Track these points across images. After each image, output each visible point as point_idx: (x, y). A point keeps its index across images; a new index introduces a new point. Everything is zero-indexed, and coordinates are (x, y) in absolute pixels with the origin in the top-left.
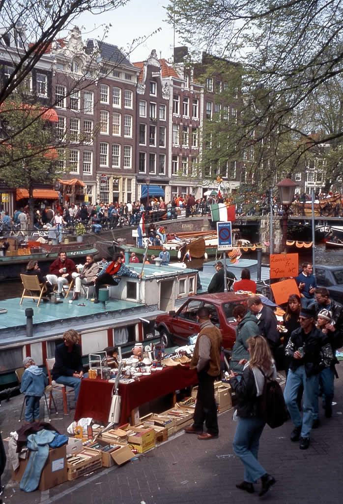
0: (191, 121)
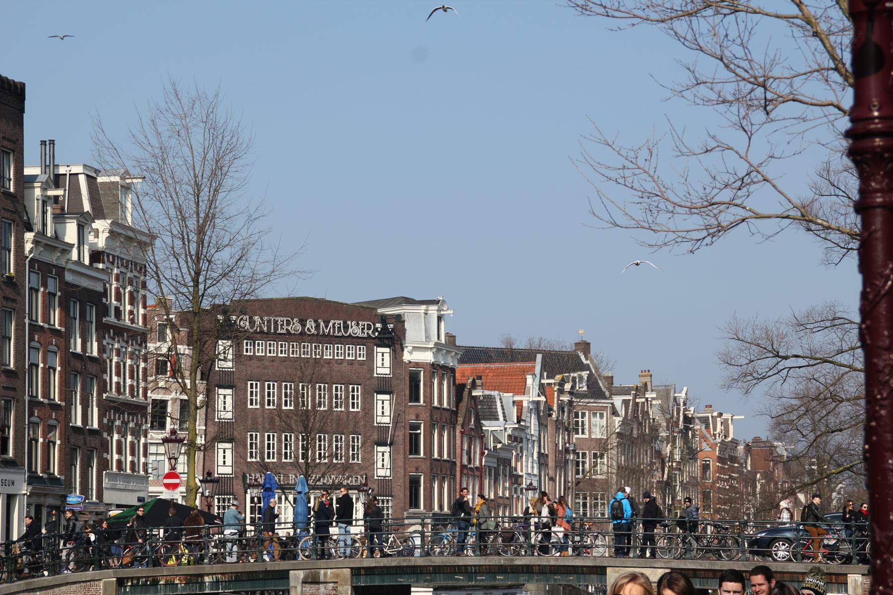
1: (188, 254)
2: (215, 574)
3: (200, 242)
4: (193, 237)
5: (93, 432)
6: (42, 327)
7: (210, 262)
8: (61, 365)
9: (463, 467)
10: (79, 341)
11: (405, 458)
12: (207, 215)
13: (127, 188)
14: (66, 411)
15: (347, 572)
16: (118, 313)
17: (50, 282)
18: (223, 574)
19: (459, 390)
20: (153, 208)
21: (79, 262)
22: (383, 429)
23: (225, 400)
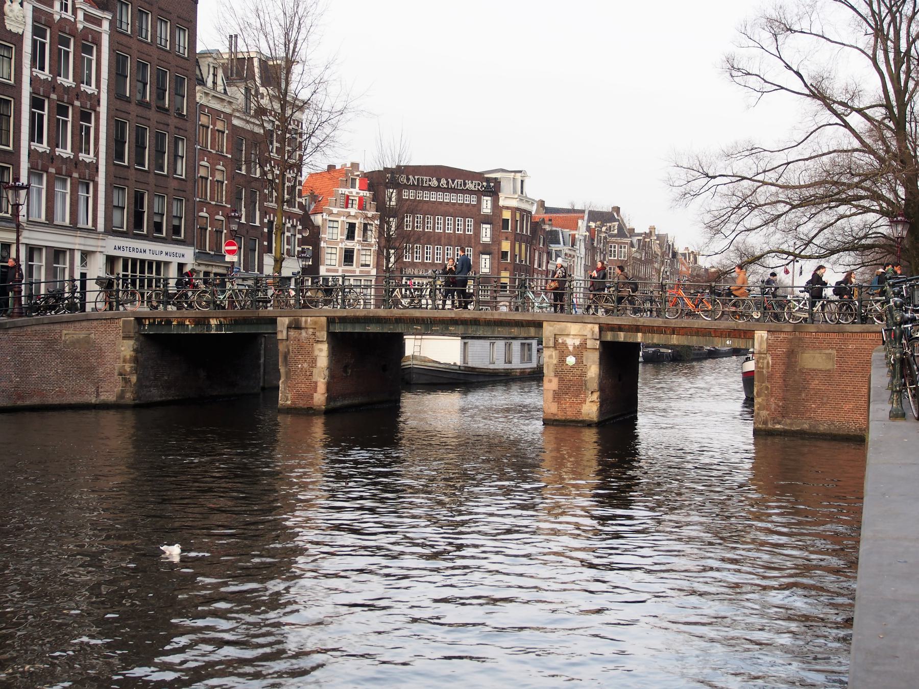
0: (79, 95)
2: (218, 318)
11: (499, 262)
15: (324, 320)
18: (225, 318)
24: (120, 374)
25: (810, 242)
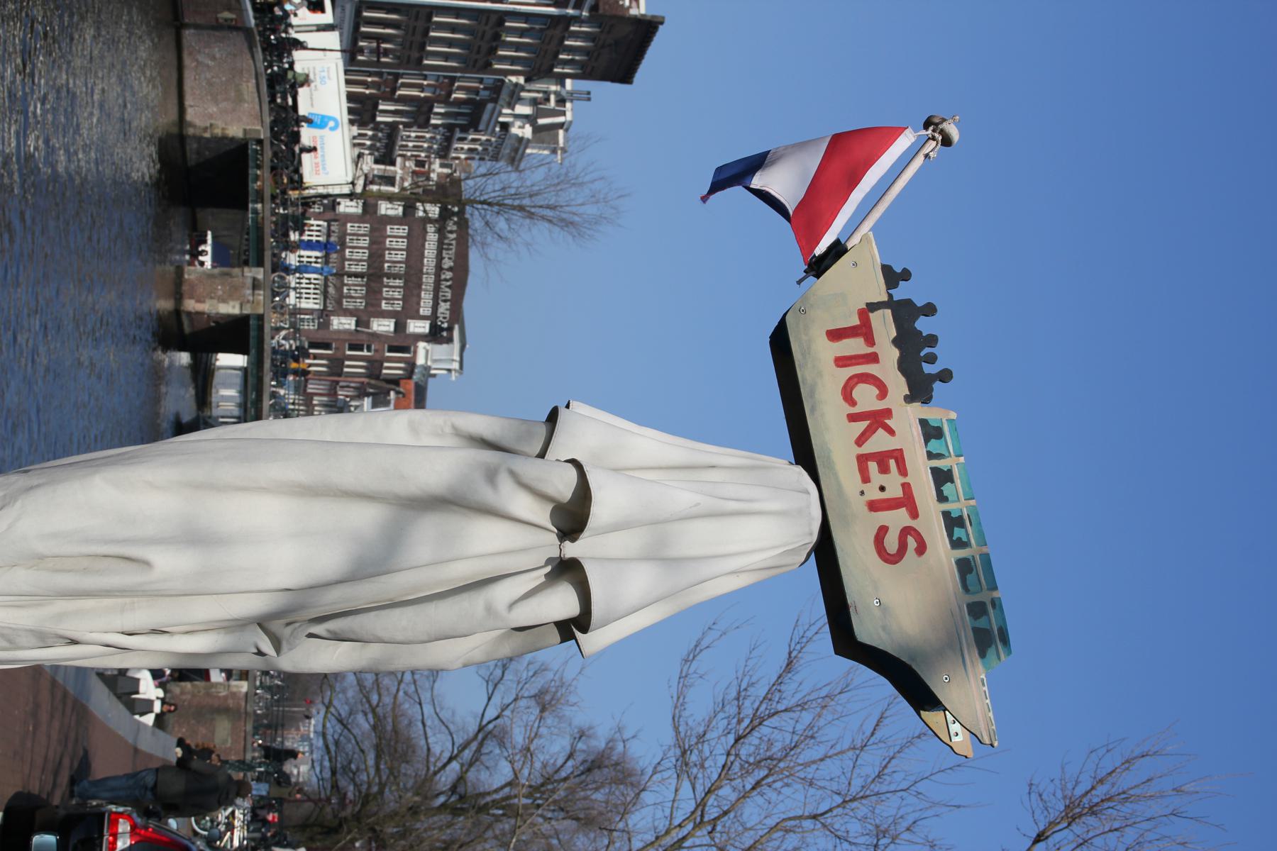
1: (505, 198)
3: (513, 208)
4: (517, 203)
5: (374, 117)
6: (453, 85)
7: (498, 213)
8: (425, 97)
9: (337, 382)
10: (442, 111)
11: (345, 341)
12: (533, 214)
13: (554, 151)
14: (390, 98)
15: (261, 311)
16: (462, 140)
17: (487, 93)
19: (394, 381)
20: (539, 175)
21: (500, 114)
22: (368, 325)
23: (396, 210)
24: (211, 125)
25: (345, 726)
